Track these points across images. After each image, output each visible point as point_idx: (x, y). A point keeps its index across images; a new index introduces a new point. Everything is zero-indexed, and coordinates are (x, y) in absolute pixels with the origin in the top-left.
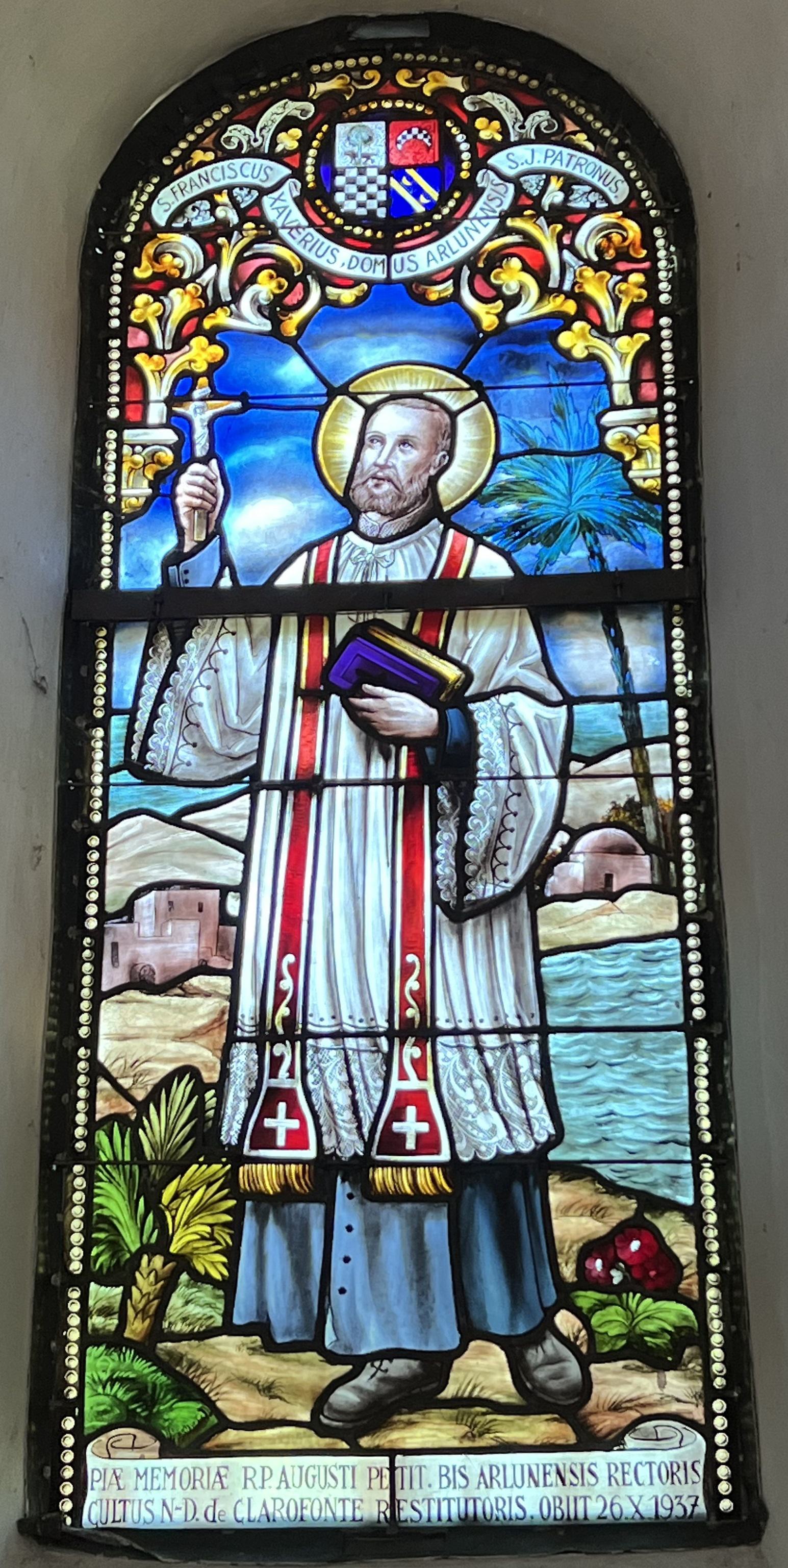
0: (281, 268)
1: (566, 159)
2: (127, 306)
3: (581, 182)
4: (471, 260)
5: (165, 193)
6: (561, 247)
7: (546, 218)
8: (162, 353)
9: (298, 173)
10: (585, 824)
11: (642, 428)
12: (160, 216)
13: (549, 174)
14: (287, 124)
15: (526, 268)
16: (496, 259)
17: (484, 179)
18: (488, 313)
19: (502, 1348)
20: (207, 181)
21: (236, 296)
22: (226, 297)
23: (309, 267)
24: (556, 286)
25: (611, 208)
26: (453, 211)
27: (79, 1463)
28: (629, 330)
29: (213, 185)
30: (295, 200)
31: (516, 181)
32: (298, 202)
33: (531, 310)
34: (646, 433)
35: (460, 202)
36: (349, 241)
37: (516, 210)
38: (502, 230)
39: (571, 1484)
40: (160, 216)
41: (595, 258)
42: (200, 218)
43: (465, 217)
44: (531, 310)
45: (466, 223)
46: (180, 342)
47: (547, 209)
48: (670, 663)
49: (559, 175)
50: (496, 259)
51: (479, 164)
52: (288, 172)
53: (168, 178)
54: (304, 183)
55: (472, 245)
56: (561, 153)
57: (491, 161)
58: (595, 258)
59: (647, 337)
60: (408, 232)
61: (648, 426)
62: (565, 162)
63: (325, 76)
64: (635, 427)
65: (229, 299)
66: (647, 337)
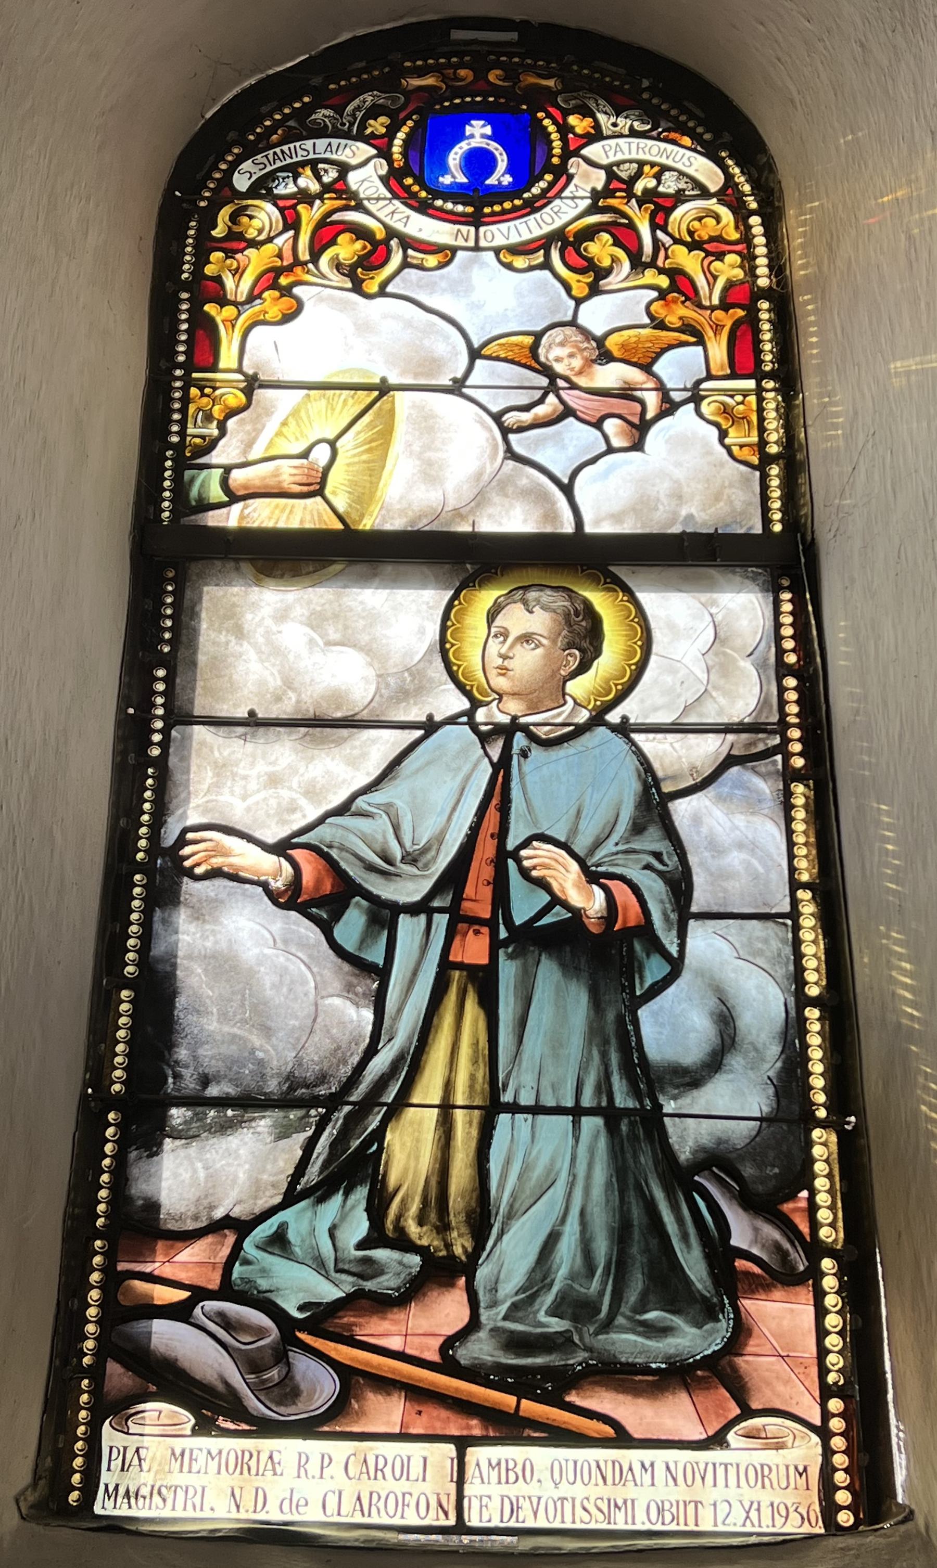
0: (361, 232)
1: (626, 150)
2: (202, 259)
3: (670, 169)
4: (558, 236)
5: (247, 165)
6: (654, 227)
7: (637, 202)
8: (235, 304)
9: (385, 153)
10: (700, 794)
11: (739, 398)
12: (241, 182)
13: (641, 164)
14: (374, 112)
15: (617, 243)
16: (589, 233)
17: (574, 165)
18: (579, 281)
19: (369, 1219)
20: (668, 157)
21: (315, 257)
22: (304, 255)
23: (391, 233)
24: (649, 260)
25: (705, 193)
26: (545, 192)
27: (94, 1440)
28: (725, 306)
29: (670, 162)
30: (381, 178)
31: (609, 170)
32: (384, 180)
33: (622, 281)
34: (742, 403)
35: (551, 185)
36: (430, 211)
37: (608, 192)
38: (594, 209)
39: (602, 1499)
40: (241, 182)
41: (689, 239)
42: (286, 188)
43: (558, 195)
44: (622, 281)
45: (557, 202)
46: (252, 298)
47: (639, 193)
48: (778, 625)
49: (653, 165)
50: (589, 233)
51: (567, 154)
52: (374, 152)
53: (249, 152)
54: (390, 161)
55: (558, 224)
56: (617, 144)
57: (584, 152)
58: (689, 239)
59: (741, 313)
60: (497, 208)
61: (745, 396)
62: (627, 151)
63: (421, 73)
64: (732, 396)
65: (307, 257)
66: (741, 313)
